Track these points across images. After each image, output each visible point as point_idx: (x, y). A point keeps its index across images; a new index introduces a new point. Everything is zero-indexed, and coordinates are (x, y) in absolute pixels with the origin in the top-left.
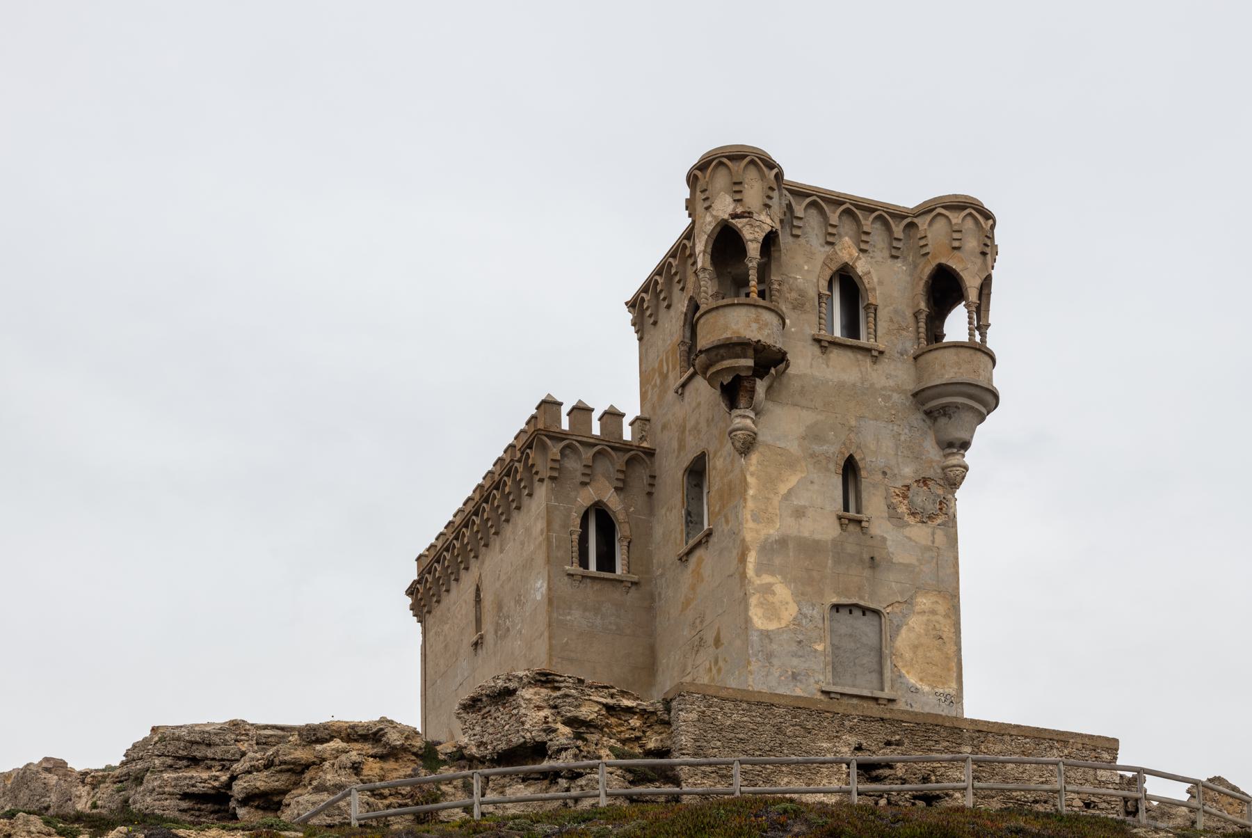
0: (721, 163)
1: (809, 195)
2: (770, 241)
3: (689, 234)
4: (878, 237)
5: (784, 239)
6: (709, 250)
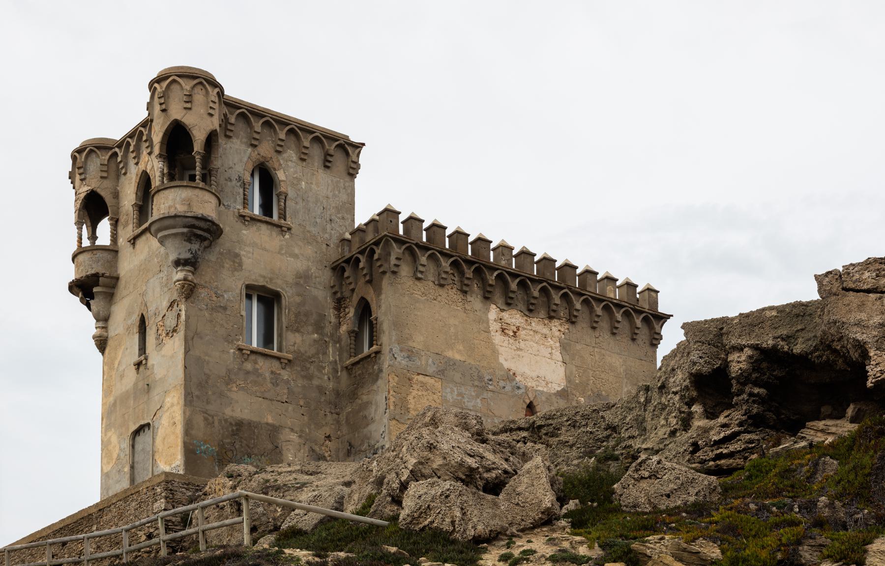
0: (201, 83)
1: (240, 108)
2: (211, 140)
3: (146, 124)
4: (316, 153)
5: (222, 140)
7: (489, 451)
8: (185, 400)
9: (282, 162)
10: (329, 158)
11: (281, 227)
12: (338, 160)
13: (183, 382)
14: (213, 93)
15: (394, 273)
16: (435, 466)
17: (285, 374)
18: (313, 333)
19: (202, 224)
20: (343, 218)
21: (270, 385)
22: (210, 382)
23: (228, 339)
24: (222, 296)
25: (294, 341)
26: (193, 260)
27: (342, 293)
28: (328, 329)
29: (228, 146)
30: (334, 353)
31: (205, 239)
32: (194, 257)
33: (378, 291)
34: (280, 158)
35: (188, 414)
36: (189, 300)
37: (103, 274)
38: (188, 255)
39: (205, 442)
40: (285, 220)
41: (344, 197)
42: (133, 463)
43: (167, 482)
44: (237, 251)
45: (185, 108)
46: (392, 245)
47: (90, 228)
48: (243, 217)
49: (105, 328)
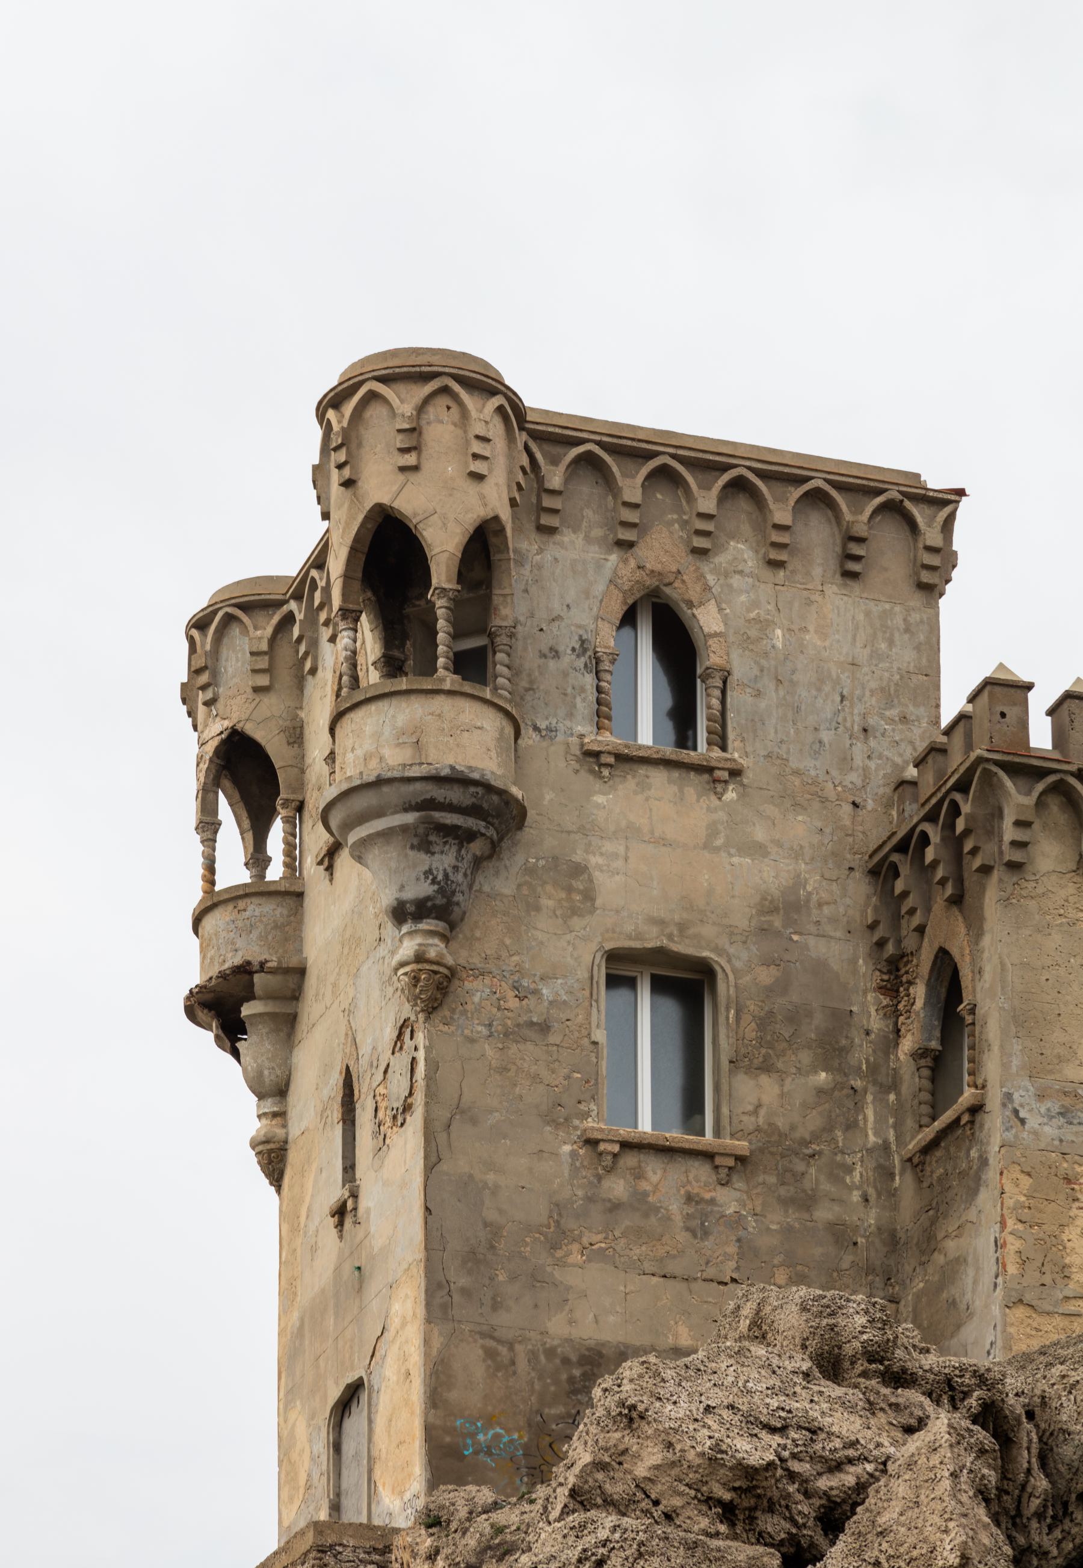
0: (445, 390)
2: (483, 547)
5: (521, 542)
6: (359, 575)
7: (852, 1409)
8: (428, 1305)
9: (711, 579)
10: (856, 549)
11: (710, 770)
12: (888, 548)
13: (420, 1255)
14: (483, 412)
15: (1014, 867)
16: (641, 1471)
17: (729, 1200)
18: (815, 1070)
19: (454, 795)
20: (904, 719)
21: (683, 1237)
22: (501, 1246)
23: (556, 1116)
24: (536, 992)
25: (753, 1101)
26: (440, 901)
27: (899, 942)
28: (862, 1053)
29: (548, 556)
30: (880, 1119)
31: (470, 836)
32: (441, 891)
33: (976, 927)
34: (705, 568)
35: (437, 1343)
36: (436, 1017)
37: (262, 965)
38: (426, 889)
39: (490, 1422)
40: (724, 748)
41: (905, 656)
42: (338, 1495)
43: (322, 1550)
44: (578, 857)
45: (403, 469)
46: (1002, 785)
47: (249, 836)
48: (597, 755)
49: (280, 1115)
